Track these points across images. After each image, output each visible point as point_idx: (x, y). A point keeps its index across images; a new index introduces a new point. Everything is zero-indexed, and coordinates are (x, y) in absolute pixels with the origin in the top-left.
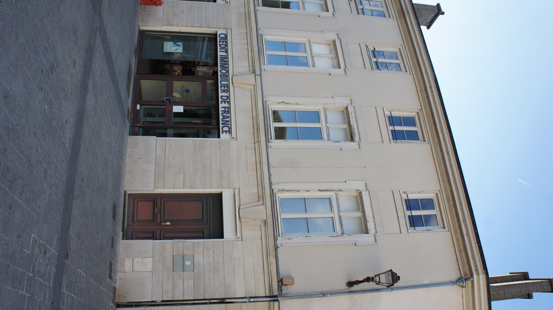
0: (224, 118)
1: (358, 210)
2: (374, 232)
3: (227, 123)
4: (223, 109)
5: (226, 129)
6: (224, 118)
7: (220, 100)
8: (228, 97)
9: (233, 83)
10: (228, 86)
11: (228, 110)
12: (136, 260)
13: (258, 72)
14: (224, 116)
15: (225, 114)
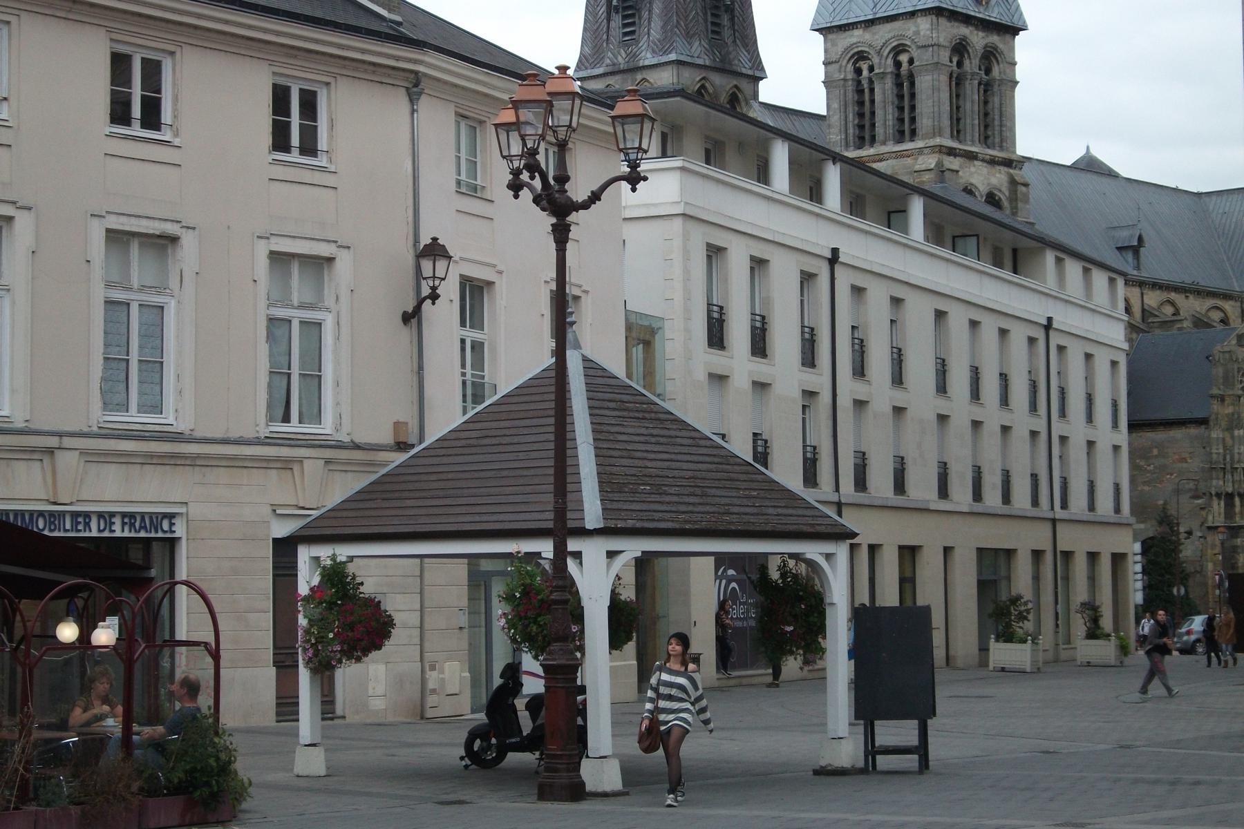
0: (145, 528)
1: (128, 244)
2: (333, 245)
3: (155, 520)
4: (127, 528)
5: (166, 526)
6: (145, 528)
7: (106, 534)
8: (100, 515)
9: (71, 504)
10: (75, 515)
11: (128, 518)
12: (370, 693)
13: (53, 442)
14: (141, 528)
15: (137, 525)
